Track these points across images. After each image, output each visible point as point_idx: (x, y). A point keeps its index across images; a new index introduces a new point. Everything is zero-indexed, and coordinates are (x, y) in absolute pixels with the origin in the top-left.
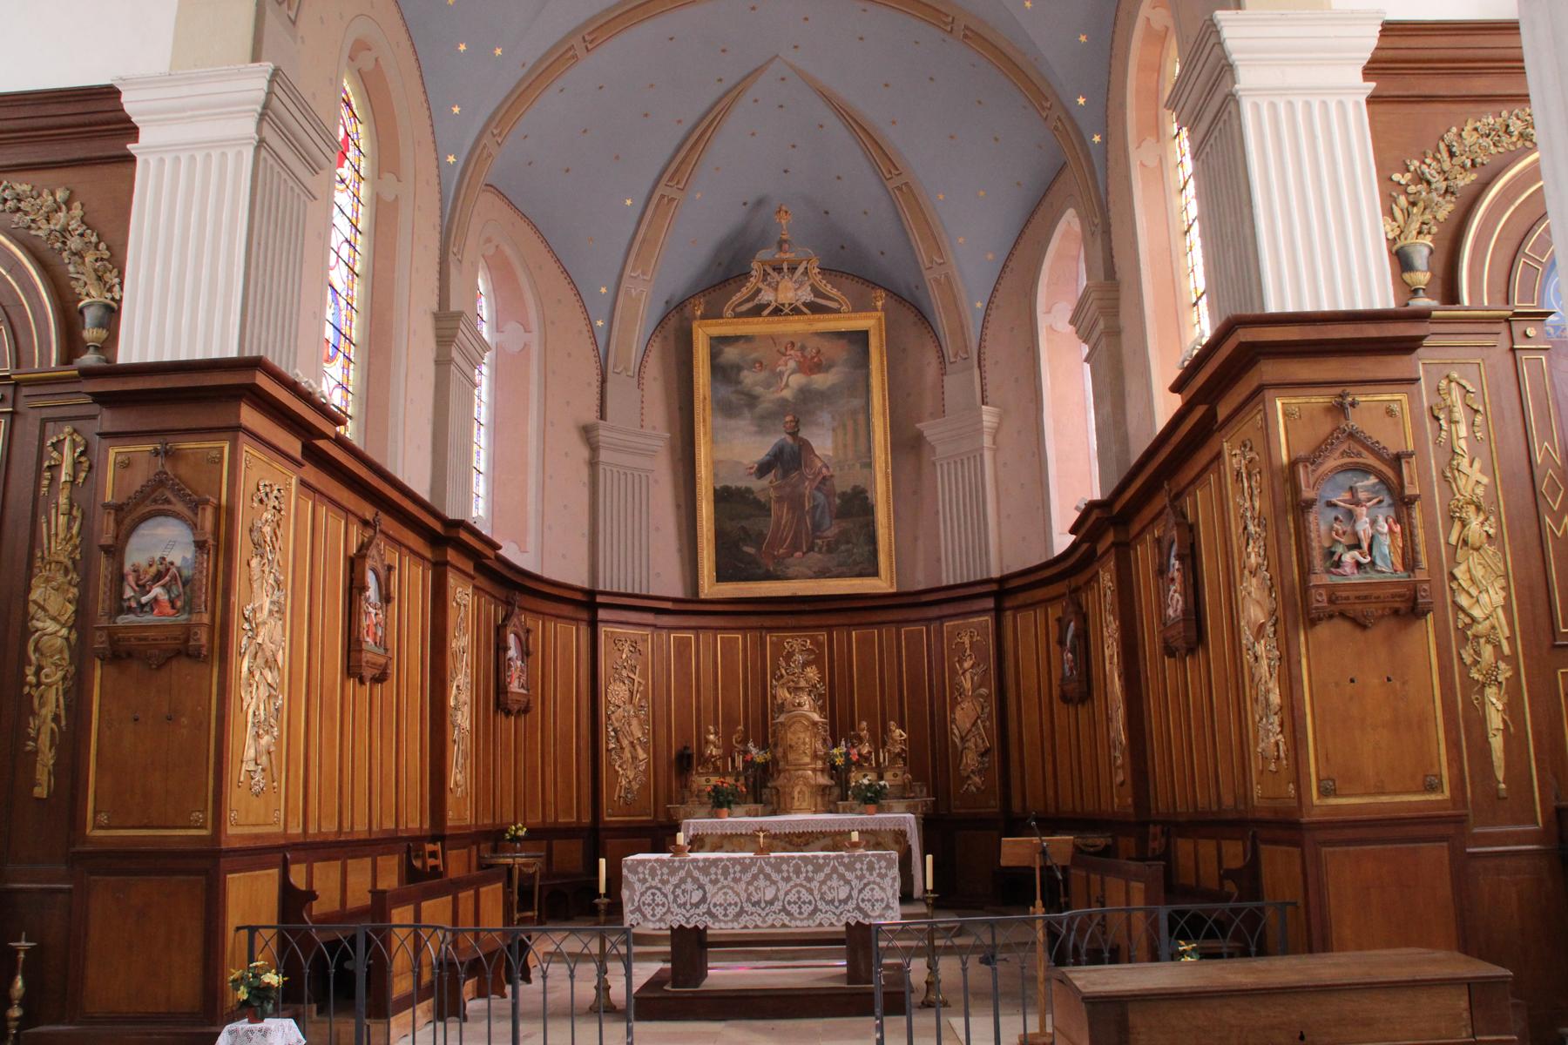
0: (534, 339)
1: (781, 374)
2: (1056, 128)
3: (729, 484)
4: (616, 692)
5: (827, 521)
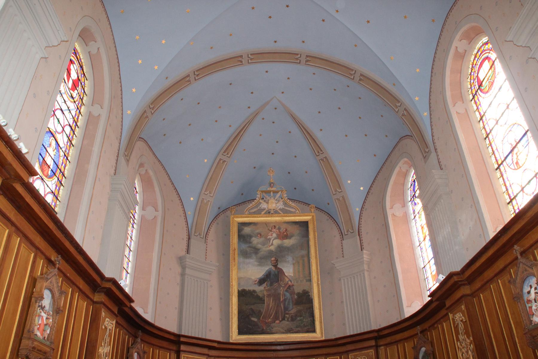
0: (159, 214)
1: (270, 239)
2: (403, 115)
5: (291, 306)
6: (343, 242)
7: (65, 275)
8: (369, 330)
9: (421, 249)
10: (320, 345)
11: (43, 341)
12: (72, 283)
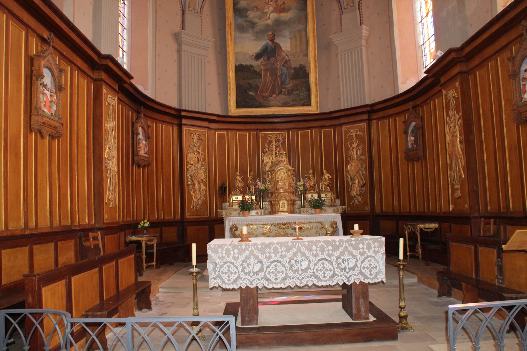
1: (266, 13)
3: (242, 63)
4: (191, 158)
6: (342, 16)
7: (61, 54)
8: (363, 104)
9: (423, 25)
10: (315, 117)
11: (52, 117)
12: (70, 62)
